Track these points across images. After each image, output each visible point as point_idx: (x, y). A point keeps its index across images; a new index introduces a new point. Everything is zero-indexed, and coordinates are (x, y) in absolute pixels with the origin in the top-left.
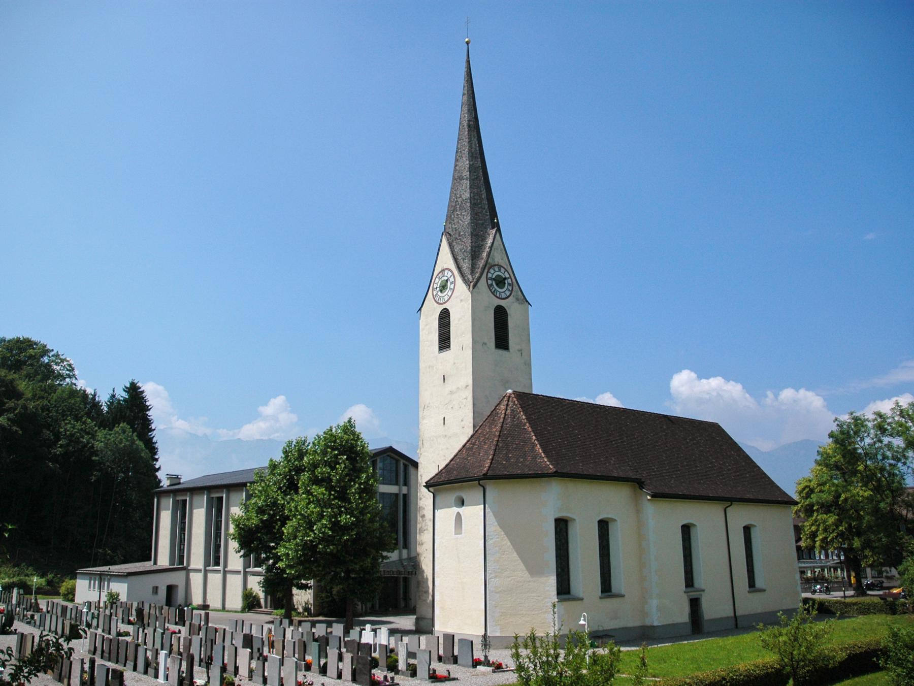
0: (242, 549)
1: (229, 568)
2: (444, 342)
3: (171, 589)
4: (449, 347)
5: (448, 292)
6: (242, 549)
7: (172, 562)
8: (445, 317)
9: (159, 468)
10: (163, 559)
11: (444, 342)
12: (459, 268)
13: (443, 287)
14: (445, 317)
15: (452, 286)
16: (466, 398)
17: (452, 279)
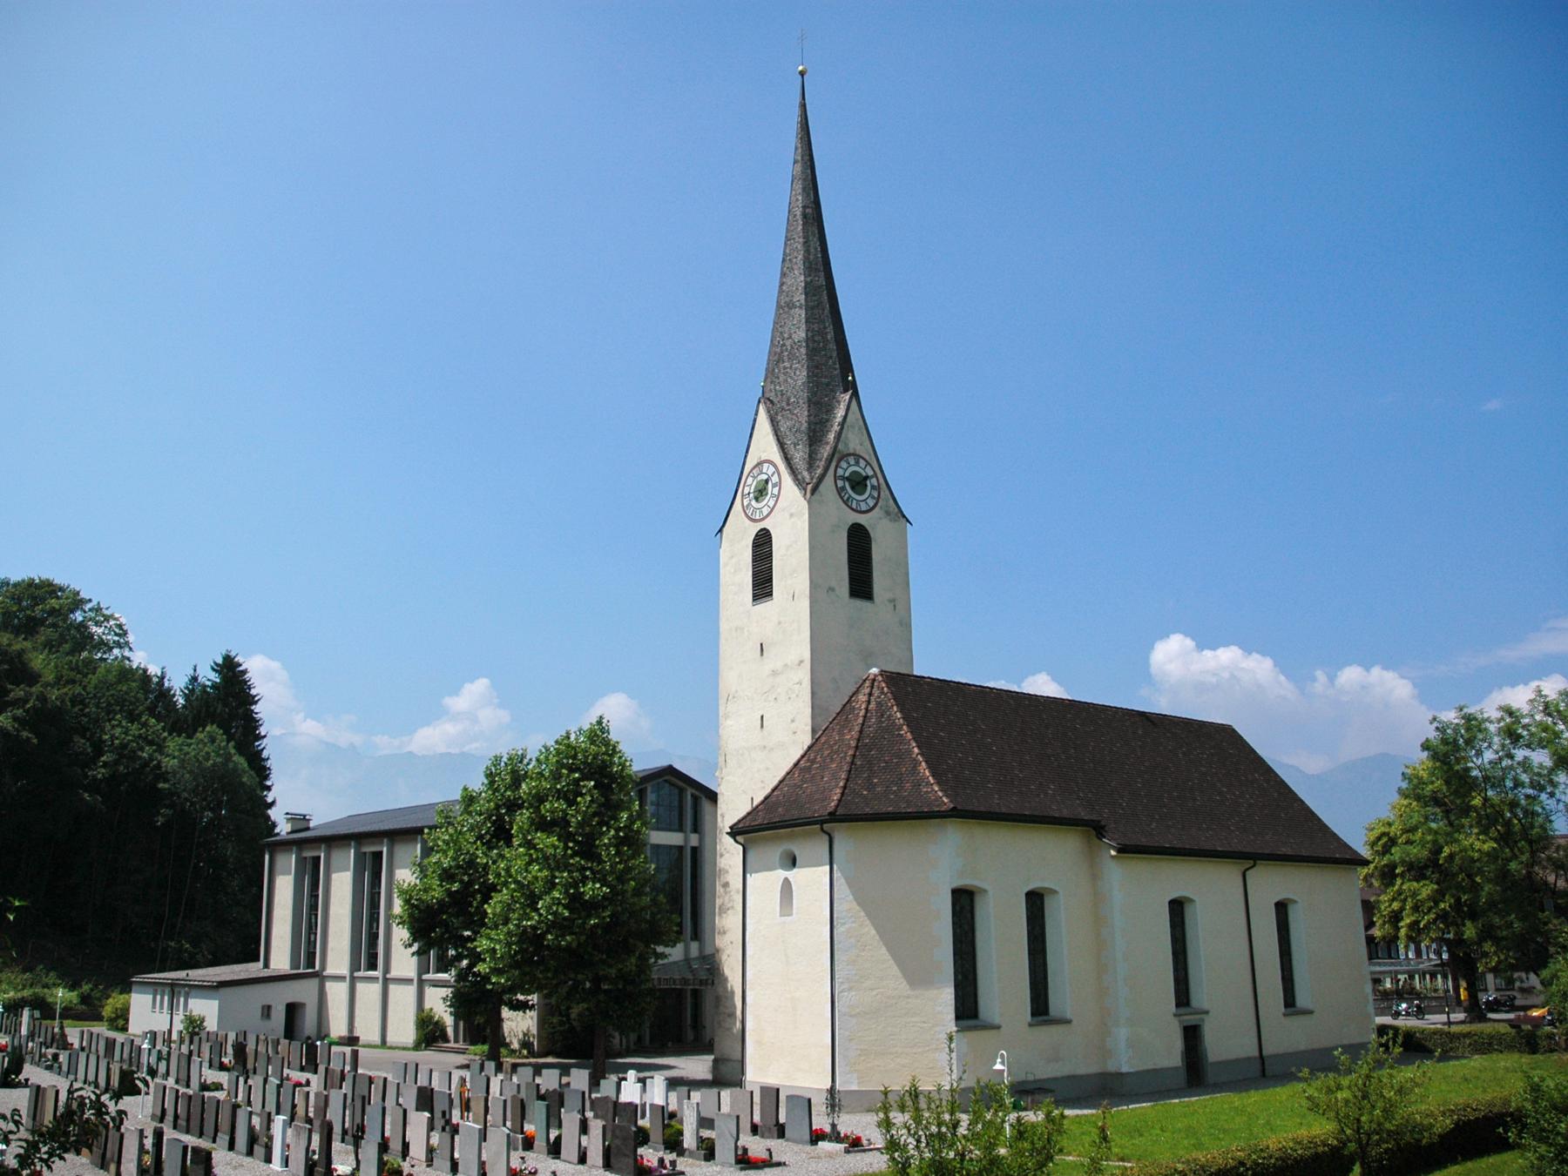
0: (415, 940)
1: (394, 973)
2: (763, 586)
3: (293, 1010)
4: (770, 594)
5: (768, 501)
6: (415, 940)
7: (295, 963)
8: (763, 543)
9: (273, 803)
10: (280, 958)
11: (763, 586)
12: (788, 460)
13: (761, 493)
14: (763, 543)
15: (776, 491)
16: (800, 683)
17: (775, 479)
